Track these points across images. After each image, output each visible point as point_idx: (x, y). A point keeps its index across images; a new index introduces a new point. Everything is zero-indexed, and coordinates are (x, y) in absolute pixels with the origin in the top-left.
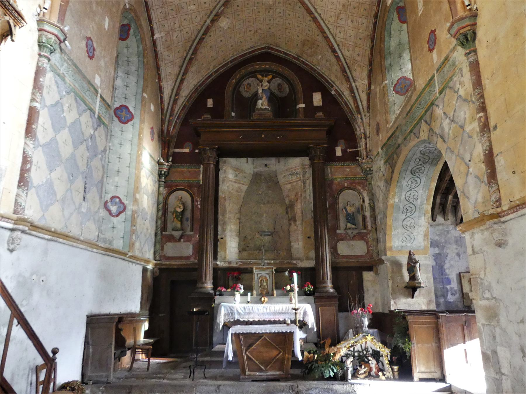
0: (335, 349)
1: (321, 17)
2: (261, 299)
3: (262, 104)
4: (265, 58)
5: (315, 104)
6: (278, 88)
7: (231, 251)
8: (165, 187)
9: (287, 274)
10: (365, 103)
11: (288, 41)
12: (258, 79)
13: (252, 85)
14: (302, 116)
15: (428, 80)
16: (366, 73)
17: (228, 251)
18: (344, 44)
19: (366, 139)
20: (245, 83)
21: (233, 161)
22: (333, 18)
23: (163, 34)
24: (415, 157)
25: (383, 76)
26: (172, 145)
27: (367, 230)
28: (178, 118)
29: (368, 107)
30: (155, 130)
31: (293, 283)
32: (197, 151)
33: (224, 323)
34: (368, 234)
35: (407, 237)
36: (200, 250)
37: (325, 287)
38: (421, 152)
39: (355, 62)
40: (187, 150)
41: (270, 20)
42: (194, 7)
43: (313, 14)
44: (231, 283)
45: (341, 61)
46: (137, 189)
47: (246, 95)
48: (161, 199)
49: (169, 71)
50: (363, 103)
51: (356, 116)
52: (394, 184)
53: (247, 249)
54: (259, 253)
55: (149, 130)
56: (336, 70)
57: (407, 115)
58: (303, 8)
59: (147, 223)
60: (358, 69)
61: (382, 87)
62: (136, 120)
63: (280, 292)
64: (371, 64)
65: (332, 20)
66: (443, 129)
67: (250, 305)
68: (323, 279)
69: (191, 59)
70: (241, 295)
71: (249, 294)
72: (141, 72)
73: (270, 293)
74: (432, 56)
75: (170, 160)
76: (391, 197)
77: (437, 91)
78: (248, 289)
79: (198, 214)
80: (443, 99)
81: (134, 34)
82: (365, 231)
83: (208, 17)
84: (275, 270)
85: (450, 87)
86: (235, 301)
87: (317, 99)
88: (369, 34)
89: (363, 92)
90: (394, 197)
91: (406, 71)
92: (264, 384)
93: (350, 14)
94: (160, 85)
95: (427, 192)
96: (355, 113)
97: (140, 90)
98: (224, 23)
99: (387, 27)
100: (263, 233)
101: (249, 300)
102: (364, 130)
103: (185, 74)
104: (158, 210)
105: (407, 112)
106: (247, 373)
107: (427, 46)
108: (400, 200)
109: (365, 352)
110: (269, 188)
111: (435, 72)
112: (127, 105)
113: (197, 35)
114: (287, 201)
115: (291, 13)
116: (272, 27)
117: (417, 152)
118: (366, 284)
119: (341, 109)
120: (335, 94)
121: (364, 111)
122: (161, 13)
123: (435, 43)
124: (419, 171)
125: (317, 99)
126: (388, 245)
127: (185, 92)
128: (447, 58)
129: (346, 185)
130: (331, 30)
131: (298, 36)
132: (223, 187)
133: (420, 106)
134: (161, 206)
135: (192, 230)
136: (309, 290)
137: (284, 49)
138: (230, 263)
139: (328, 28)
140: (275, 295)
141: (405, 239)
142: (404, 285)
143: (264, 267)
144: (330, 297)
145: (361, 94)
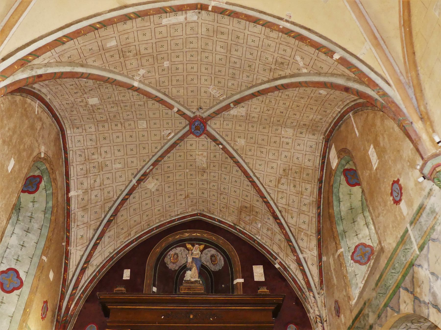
1: (260, 181)
3: (192, 275)
4: (198, 227)
5: (256, 279)
6: (211, 259)
10: (317, 279)
11: (223, 208)
12: (188, 250)
13: (179, 255)
14: (240, 291)
15: (399, 236)
16: (314, 243)
18: (287, 211)
20: (172, 252)
22: (273, 183)
23: (80, 192)
25: (336, 243)
28: (83, 293)
29: (321, 283)
39: (300, 230)
42: (119, 166)
45: (284, 229)
47: (171, 266)
49: (80, 234)
50: (314, 278)
51: (307, 294)
55: (41, 305)
56: (280, 240)
57: (377, 284)
58: (240, 171)
60: (305, 238)
61: (336, 256)
62: (26, 290)
64: (319, 232)
65: (273, 184)
66: (434, 295)
69: (109, 221)
72: (45, 231)
74: (400, 209)
77: (415, 247)
80: (426, 256)
81: (45, 189)
83: (134, 177)
85: (434, 240)
87: (259, 273)
88: (315, 200)
89: (313, 265)
91: (363, 237)
93: (292, 179)
96: (306, 290)
97: (39, 252)
98: (151, 184)
99: (335, 190)
102: (319, 311)
103: (100, 237)
105: (377, 281)
107: (391, 198)
111: (408, 226)
112: (17, 268)
113: (120, 195)
115: (227, 177)
119: (288, 286)
120: (279, 268)
121: (316, 287)
122: (82, 169)
123: (401, 193)
125: (259, 273)
127: (98, 260)
128: (421, 208)
130: (271, 195)
131: (234, 202)
133: (393, 271)
137: (219, 217)
139: (269, 194)
145: (311, 267)
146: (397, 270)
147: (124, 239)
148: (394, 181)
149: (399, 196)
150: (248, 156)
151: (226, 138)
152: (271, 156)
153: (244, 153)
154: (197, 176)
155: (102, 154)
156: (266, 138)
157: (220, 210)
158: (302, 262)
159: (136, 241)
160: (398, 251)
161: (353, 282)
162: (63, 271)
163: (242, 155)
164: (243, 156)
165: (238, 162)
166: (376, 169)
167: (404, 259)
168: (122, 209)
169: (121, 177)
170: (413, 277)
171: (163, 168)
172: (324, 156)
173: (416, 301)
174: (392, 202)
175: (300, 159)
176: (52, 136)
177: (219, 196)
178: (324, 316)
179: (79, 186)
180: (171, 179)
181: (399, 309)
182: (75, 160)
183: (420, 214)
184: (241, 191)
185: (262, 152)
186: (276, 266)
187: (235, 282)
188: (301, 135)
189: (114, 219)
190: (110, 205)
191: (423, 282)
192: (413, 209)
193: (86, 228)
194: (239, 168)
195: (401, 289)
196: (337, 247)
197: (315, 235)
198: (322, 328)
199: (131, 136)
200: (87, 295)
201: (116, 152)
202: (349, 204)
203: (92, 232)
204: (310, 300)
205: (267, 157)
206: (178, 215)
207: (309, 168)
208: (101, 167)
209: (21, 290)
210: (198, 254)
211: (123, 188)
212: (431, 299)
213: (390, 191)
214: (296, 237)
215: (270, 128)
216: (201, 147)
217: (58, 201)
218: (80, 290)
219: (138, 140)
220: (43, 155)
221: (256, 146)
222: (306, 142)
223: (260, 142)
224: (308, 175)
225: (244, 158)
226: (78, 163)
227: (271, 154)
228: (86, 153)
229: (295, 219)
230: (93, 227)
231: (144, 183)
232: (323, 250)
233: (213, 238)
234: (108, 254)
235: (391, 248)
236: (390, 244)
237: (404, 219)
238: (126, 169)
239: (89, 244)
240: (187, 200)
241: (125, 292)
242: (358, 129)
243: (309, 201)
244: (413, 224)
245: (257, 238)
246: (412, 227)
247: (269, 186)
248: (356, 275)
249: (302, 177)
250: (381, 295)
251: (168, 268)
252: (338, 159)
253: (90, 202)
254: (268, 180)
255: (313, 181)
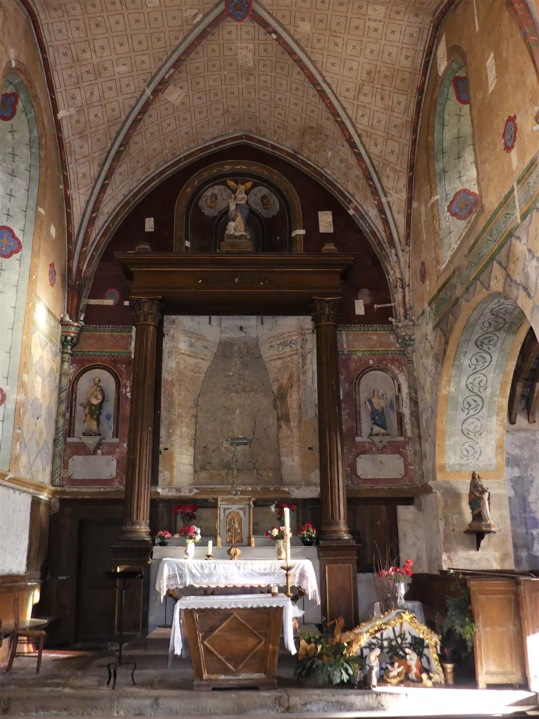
0: (350, 635)
2: (229, 552)
3: (236, 227)
4: (243, 155)
5: (322, 230)
6: (262, 201)
7: (180, 471)
8: (72, 363)
9: (273, 509)
10: (402, 232)
13: (219, 196)
14: (300, 248)
15: (503, 195)
16: (403, 181)
17: (175, 470)
19: (403, 288)
20: (209, 193)
21: (187, 321)
23: (73, 111)
24: (482, 319)
25: (431, 187)
26: (86, 292)
27: (406, 436)
28: (96, 250)
29: (408, 237)
30: (57, 268)
31: (283, 525)
32: (126, 303)
33: (168, 592)
34: (406, 443)
35: (469, 449)
36: (129, 467)
37: (336, 532)
38: (491, 311)
40: (110, 302)
41: (249, 93)
42: (124, 69)
43: (319, 84)
44: (180, 524)
45: (364, 162)
46: (25, 366)
47: (208, 212)
48: (65, 382)
49: (82, 172)
50: (400, 230)
51: (388, 250)
52: (448, 363)
53: (208, 466)
54: (227, 474)
55: (47, 269)
57: (470, 251)
59: (41, 423)
60: (392, 175)
61: (429, 205)
62: (26, 252)
63: (262, 539)
64: (412, 167)
66: (526, 276)
67: (212, 562)
68: (333, 518)
69: (119, 153)
70: (197, 544)
71: (210, 543)
72: (35, 173)
73: (245, 541)
74: (510, 160)
75: (82, 318)
76: (443, 383)
77: (518, 214)
78: (210, 534)
79: (127, 408)
82: (402, 439)
83: (148, 86)
84: (254, 502)
86: (187, 554)
87: (326, 221)
88: (410, 119)
89: (399, 212)
90: (449, 382)
91: (468, 181)
92: (233, 695)
93: (379, 86)
94: (66, 194)
95: (501, 376)
96: (386, 245)
97: (33, 203)
98: (174, 95)
99: (439, 108)
100: (235, 441)
101: (210, 553)
102: (401, 273)
103: (108, 176)
104: (60, 402)
105: (471, 247)
106: (205, 676)
107: (503, 141)
108: (458, 389)
109: (399, 640)
110: (245, 366)
111: (515, 184)
114: (275, 387)
116: (253, 105)
117: (486, 311)
118: (402, 526)
120: (354, 215)
121: (400, 243)
122: (70, 76)
123: (515, 137)
124: (490, 341)
125: (326, 221)
126: (439, 461)
127: (109, 207)
129: (371, 362)
130: (347, 110)
131: (295, 120)
132: (170, 365)
133: (490, 238)
134: (64, 395)
135: (116, 434)
136: (310, 537)
137: (274, 141)
138: (178, 490)
139: (344, 109)
140: (253, 545)
141: (465, 453)
142: (467, 527)
143: (236, 497)
144: (342, 548)
146: (495, 238)
147: (142, 175)
148: (510, 117)
149: (512, 140)
150: (315, 51)
151: (282, 21)
152: (350, 50)
153: (310, 45)
154: (240, 80)
155: (97, 51)
156: (343, 20)
157: (274, 130)
158: (383, 208)
159: (158, 178)
160: (499, 214)
161: (446, 241)
162: (66, 223)
163: (306, 49)
164: (309, 50)
165: (301, 61)
166: (492, 93)
167: (503, 226)
168: (134, 134)
169: (128, 85)
170: (509, 251)
171: (188, 70)
172: (430, 53)
173: (508, 279)
174: (503, 147)
175: (394, 55)
176: (21, 29)
177: (272, 110)
178: (407, 280)
179: (70, 102)
180: (202, 86)
181: (489, 285)
182: (58, 62)
183: (530, 172)
184: (305, 103)
185: (336, 44)
186: (349, 212)
187: (294, 234)
188: (397, 17)
189: (125, 149)
190: (116, 128)
191: (518, 258)
192: (524, 164)
193: (87, 164)
194: (302, 69)
195: (495, 262)
196: (431, 193)
197: (405, 171)
198: (402, 294)
199: (137, 21)
200: (101, 251)
201: (117, 47)
202: (456, 131)
203: (96, 168)
204: (391, 259)
205: (344, 53)
206: (214, 138)
207: (406, 69)
208: (98, 71)
209: (20, 253)
210: (243, 198)
211: (133, 102)
212: (523, 280)
213: (503, 131)
214: (380, 173)
215: (351, 5)
216: (245, 36)
217: (44, 128)
218: (91, 246)
219: (148, 27)
220: (14, 64)
221: (327, 33)
222: (403, 29)
223: (334, 27)
224: (403, 80)
225: (309, 53)
226: (64, 66)
227: (350, 47)
228: (73, 50)
229: (379, 147)
230: (97, 162)
231: (163, 93)
232: (415, 194)
233: (265, 172)
234: (122, 197)
235: (492, 208)
236: (492, 203)
237: (512, 174)
238: (135, 73)
239: (95, 185)
240: (226, 117)
241: (150, 250)
242: (478, 20)
243: (401, 121)
244: (521, 184)
245: (326, 172)
246: (519, 187)
247: (345, 97)
248: (450, 233)
249: (394, 85)
250: (473, 264)
251: (204, 214)
252: (448, 60)
253: (88, 125)
254: (343, 89)
255: (409, 91)
